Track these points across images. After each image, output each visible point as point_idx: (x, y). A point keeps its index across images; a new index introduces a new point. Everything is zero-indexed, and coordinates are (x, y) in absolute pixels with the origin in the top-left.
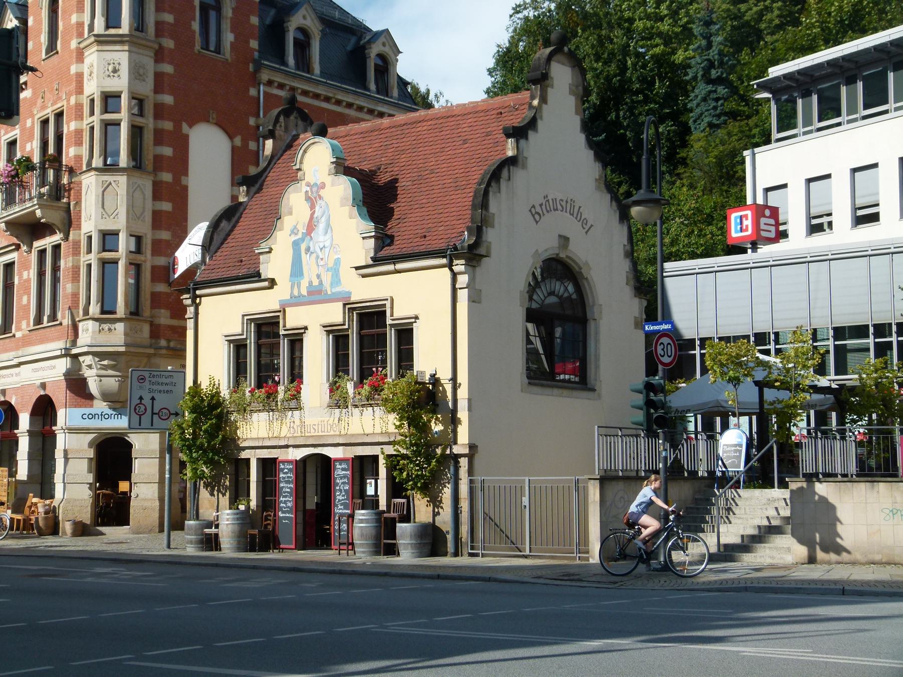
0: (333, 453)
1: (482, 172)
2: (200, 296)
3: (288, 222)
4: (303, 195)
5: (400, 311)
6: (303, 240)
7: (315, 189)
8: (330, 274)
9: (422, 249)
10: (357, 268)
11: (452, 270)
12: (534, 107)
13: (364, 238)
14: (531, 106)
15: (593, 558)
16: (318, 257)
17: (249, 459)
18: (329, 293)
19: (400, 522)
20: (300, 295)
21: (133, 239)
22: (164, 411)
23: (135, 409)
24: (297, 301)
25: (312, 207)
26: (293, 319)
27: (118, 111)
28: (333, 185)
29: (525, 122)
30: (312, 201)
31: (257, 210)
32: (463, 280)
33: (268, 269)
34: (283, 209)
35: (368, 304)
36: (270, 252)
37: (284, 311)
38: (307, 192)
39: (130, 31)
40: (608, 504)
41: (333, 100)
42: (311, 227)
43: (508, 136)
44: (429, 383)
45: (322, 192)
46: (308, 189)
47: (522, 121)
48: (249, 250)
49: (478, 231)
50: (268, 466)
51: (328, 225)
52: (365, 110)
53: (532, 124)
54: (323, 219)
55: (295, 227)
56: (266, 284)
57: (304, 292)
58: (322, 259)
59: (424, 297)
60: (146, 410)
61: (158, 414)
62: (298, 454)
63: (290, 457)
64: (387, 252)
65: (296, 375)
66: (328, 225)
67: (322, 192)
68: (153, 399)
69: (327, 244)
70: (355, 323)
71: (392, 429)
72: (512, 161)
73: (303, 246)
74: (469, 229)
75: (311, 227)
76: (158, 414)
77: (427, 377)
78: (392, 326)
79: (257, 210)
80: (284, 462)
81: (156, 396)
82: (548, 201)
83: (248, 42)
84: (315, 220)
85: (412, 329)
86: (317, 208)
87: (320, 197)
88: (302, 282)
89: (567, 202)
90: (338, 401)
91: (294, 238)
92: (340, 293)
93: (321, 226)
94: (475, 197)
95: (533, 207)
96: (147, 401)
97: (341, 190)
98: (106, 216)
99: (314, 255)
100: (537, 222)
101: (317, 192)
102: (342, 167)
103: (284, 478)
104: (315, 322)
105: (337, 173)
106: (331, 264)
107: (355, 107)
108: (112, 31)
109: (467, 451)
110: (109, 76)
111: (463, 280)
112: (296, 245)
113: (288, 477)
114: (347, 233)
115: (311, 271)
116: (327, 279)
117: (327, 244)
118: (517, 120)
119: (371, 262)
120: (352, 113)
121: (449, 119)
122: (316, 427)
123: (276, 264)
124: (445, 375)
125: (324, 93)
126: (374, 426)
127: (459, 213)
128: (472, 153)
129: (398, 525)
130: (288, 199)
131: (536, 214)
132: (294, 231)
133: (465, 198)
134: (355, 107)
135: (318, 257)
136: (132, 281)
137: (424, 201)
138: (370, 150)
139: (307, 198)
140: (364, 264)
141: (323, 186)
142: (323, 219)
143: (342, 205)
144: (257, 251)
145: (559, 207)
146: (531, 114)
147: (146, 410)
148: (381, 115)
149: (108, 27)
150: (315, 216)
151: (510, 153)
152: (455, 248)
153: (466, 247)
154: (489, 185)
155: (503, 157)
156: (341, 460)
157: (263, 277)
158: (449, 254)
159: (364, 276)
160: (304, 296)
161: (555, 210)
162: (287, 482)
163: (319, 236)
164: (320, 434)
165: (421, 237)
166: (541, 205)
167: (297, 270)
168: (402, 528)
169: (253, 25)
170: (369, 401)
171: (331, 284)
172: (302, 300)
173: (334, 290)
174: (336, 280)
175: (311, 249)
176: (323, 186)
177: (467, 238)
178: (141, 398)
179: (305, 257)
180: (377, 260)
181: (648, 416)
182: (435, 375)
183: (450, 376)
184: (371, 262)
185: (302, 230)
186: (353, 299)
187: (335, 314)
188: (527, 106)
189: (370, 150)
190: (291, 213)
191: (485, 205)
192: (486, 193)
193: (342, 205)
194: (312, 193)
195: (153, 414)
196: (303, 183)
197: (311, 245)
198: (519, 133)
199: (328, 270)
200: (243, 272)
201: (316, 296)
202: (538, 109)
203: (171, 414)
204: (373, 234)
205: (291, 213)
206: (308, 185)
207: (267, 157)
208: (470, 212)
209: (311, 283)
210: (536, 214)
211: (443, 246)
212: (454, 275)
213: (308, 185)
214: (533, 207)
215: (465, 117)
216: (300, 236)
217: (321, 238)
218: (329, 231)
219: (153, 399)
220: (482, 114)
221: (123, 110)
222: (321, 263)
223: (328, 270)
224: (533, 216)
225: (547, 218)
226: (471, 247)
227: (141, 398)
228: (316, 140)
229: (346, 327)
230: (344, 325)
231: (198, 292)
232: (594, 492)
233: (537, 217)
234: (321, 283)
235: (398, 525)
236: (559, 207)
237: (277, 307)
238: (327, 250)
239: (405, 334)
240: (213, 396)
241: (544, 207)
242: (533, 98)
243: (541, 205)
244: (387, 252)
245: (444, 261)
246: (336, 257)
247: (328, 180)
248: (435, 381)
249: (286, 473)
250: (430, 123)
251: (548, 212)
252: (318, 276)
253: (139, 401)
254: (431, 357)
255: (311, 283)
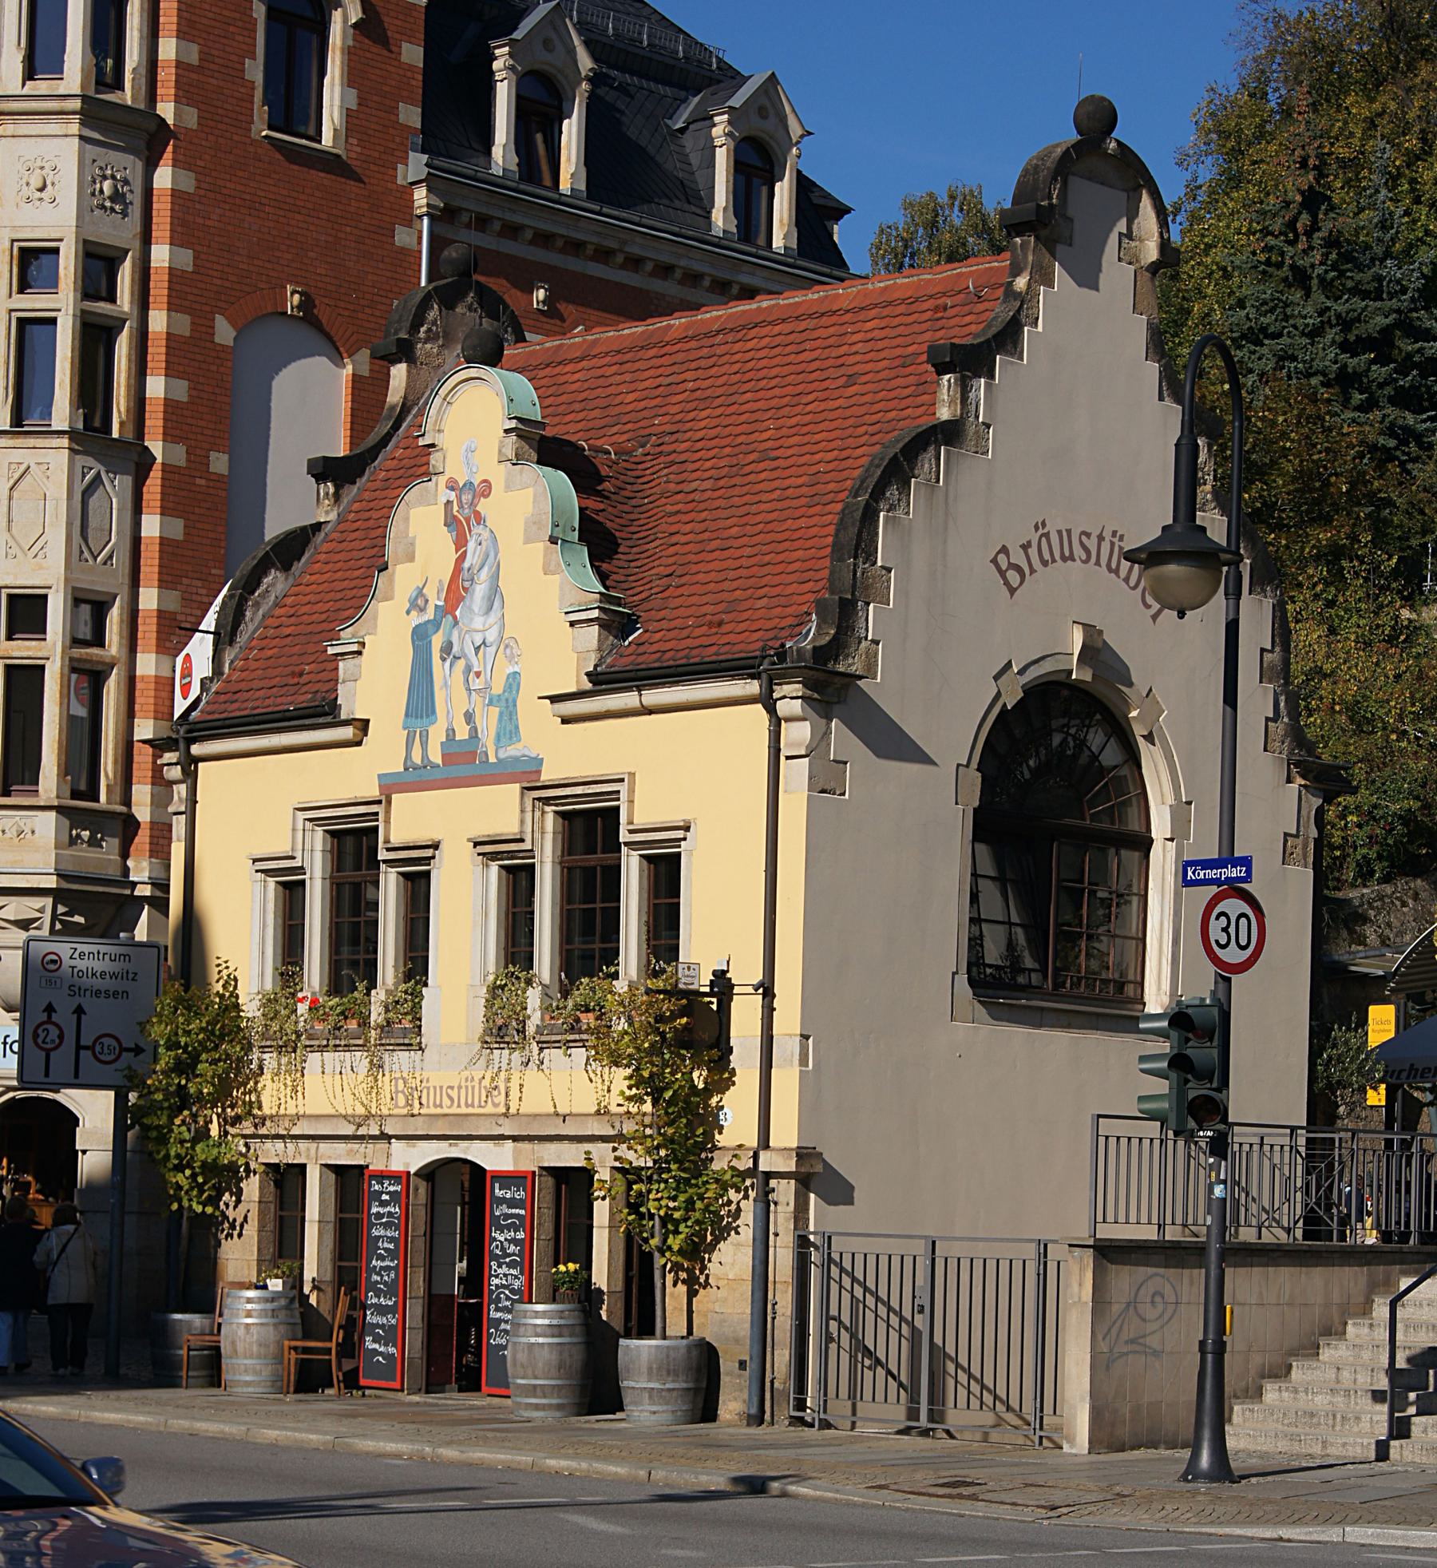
0: (494, 1158)
1: (865, 461)
2: (197, 760)
3: (402, 579)
4: (439, 511)
5: (644, 811)
6: (436, 624)
7: (466, 498)
8: (495, 711)
9: (709, 654)
10: (554, 699)
11: (771, 709)
12: (1017, 295)
13: (572, 624)
14: (1010, 292)
15: (1072, 1441)
16: (468, 669)
17: (303, 1167)
18: (492, 759)
19: (628, 1335)
20: (427, 764)
21: (86, 609)
22: (107, 1041)
23: (36, 1035)
24: (415, 779)
25: (460, 543)
26: (406, 822)
27: (51, 283)
28: (508, 488)
29: (994, 330)
30: (459, 526)
31: (357, 545)
32: (798, 735)
33: (354, 700)
34: (393, 549)
35: (579, 790)
36: (359, 653)
37: (389, 802)
38: (449, 503)
39: (83, 87)
40: (1116, 1308)
41: (620, 259)
42: (456, 592)
43: (941, 370)
44: (710, 994)
45: (483, 506)
46: (453, 496)
47: (989, 326)
48: (311, 648)
49: (844, 614)
50: (349, 1182)
51: (495, 590)
52: (707, 283)
53: (1008, 337)
54: (484, 574)
55: (420, 592)
56: (347, 733)
57: (436, 757)
58: (478, 674)
59: (705, 773)
60: (61, 1037)
61: (92, 1048)
62: (410, 1158)
63: (396, 1166)
64: (633, 662)
65: (416, 966)
66: (495, 590)
67: (483, 506)
68: (79, 1011)
69: (491, 636)
70: (549, 837)
71: (614, 1102)
72: (951, 433)
73: (437, 641)
74: (821, 607)
75: (456, 592)
76: (92, 1048)
77: (706, 978)
78: (390, 863)
79: (357, 545)
80: (381, 1176)
81: (87, 1003)
82: (1047, 535)
83: (394, 111)
84: (465, 574)
85: (677, 856)
86: (471, 545)
87: (479, 519)
88: (431, 730)
89: (1101, 538)
90: (503, 1031)
91: (416, 619)
92: (516, 759)
93: (480, 590)
94: (841, 526)
95: (1004, 550)
96: (64, 1017)
97: (528, 503)
98: (15, 550)
99: (461, 663)
100: (1012, 591)
101: (472, 504)
102: (544, 446)
103: (379, 1216)
104: (454, 828)
105: (519, 459)
106: (498, 688)
107: (678, 274)
108: (40, 87)
109: (791, 1166)
110: (29, 200)
111: (798, 735)
112: (420, 636)
113: (390, 1214)
114: (539, 611)
115: (451, 696)
116: (488, 723)
117: (491, 636)
118: (968, 330)
119: (589, 686)
120: (670, 288)
121: (824, 321)
122: (454, 1094)
123: (373, 681)
124: (746, 973)
125: (595, 239)
126: (573, 1096)
127: (807, 565)
128: (863, 410)
129: (622, 1342)
130: (407, 519)
131: (1010, 572)
132: (417, 603)
133: (823, 525)
134: (678, 274)
135: (468, 669)
136: (81, 711)
137: (734, 531)
138: (631, 397)
139: (451, 521)
140: (573, 689)
141: (486, 489)
142: (484, 574)
143: (528, 540)
144: (330, 651)
145: (1079, 552)
146: (1003, 312)
147: (61, 1037)
148: (749, 293)
149: (30, 74)
150: (466, 565)
151: (944, 414)
152: (782, 655)
153: (808, 655)
154: (878, 493)
155: (926, 422)
156: (508, 1179)
157: (343, 716)
158: (766, 667)
159: (566, 721)
160: (435, 766)
161: (1064, 559)
162: (386, 1226)
163: (475, 620)
164: (464, 1110)
165: (710, 625)
166: (1025, 547)
167: (420, 702)
168: (637, 1351)
169: (411, 68)
170: (567, 1032)
171: (498, 738)
172: (427, 775)
173: (502, 755)
174: (509, 730)
175: (455, 649)
176: (486, 489)
177: (812, 635)
178: (50, 1009)
179: (439, 668)
180: (602, 681)
181: (1180, 1090)
182: (724, 972)
183: (758, 976)
184: (589, 686)
185: (435, 600)
186: (546, 776)
187: (499, 810)
188: (1000, 292)
189: (631, 397)
190: (411, 558)
191: (864, 546)
192: (869, 517)
193: (528, 540)
194: (461, 506)
195: (79, 1047)
196: (442, 480)
197: (455, 639)
198: (970, 361)
199: (491, 703)
200: (304, 699)
201: (463, 766)
202: (1025, 300)
203: (123, 1049)
204: (595, 614)
205: (411, 558)
206: (452, 486)
207: (393, 408)
208: (827, 562)
209: (451, 732)
210: (1010, 572)
211: (755, 648)
212: (776, 722)
213: (452, 486)
214: (1004, 550)
215: (862, 316)
216: (430, 614)
217: (478, 622)
218: (496, 604)
219: (79, 1011)
220: (902, 309)
221: (62, 284)
222: (477, 684)
223: (491, 703)
224: (1002, 574)
225: (1044, 582)
226: (826, 654)
227: (50, 1009)
228: (472, 373)
229: (527, 846)
230: (522, 840)
231: (196, 749)
232: (1078, 1282)
233: (1013, 577)
234: (474, 734)
235: (622, 1342)
236: (1079, 552)
237: (374, 792)
238: (491, 650)
239: (665, 872)
240: (226, 1009)
241: (1033, 551)
242: (1016, 271)
243: (1025, 547)
244: (633, 662)
245: (753, 687)
246: (510, 670)
247: (497, 474)
248: (722, 984)
249: (383, 1204)
250: (777, 329)
251: (1045, 563)
252: (469, 717)
253: (44, 1017)
254: (717, 933)
255: (451, 732)
